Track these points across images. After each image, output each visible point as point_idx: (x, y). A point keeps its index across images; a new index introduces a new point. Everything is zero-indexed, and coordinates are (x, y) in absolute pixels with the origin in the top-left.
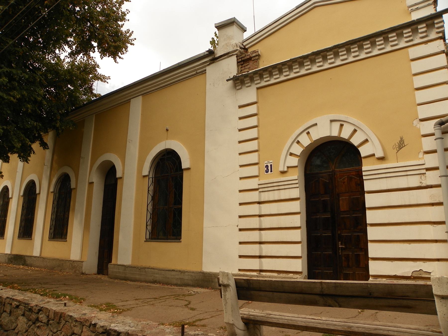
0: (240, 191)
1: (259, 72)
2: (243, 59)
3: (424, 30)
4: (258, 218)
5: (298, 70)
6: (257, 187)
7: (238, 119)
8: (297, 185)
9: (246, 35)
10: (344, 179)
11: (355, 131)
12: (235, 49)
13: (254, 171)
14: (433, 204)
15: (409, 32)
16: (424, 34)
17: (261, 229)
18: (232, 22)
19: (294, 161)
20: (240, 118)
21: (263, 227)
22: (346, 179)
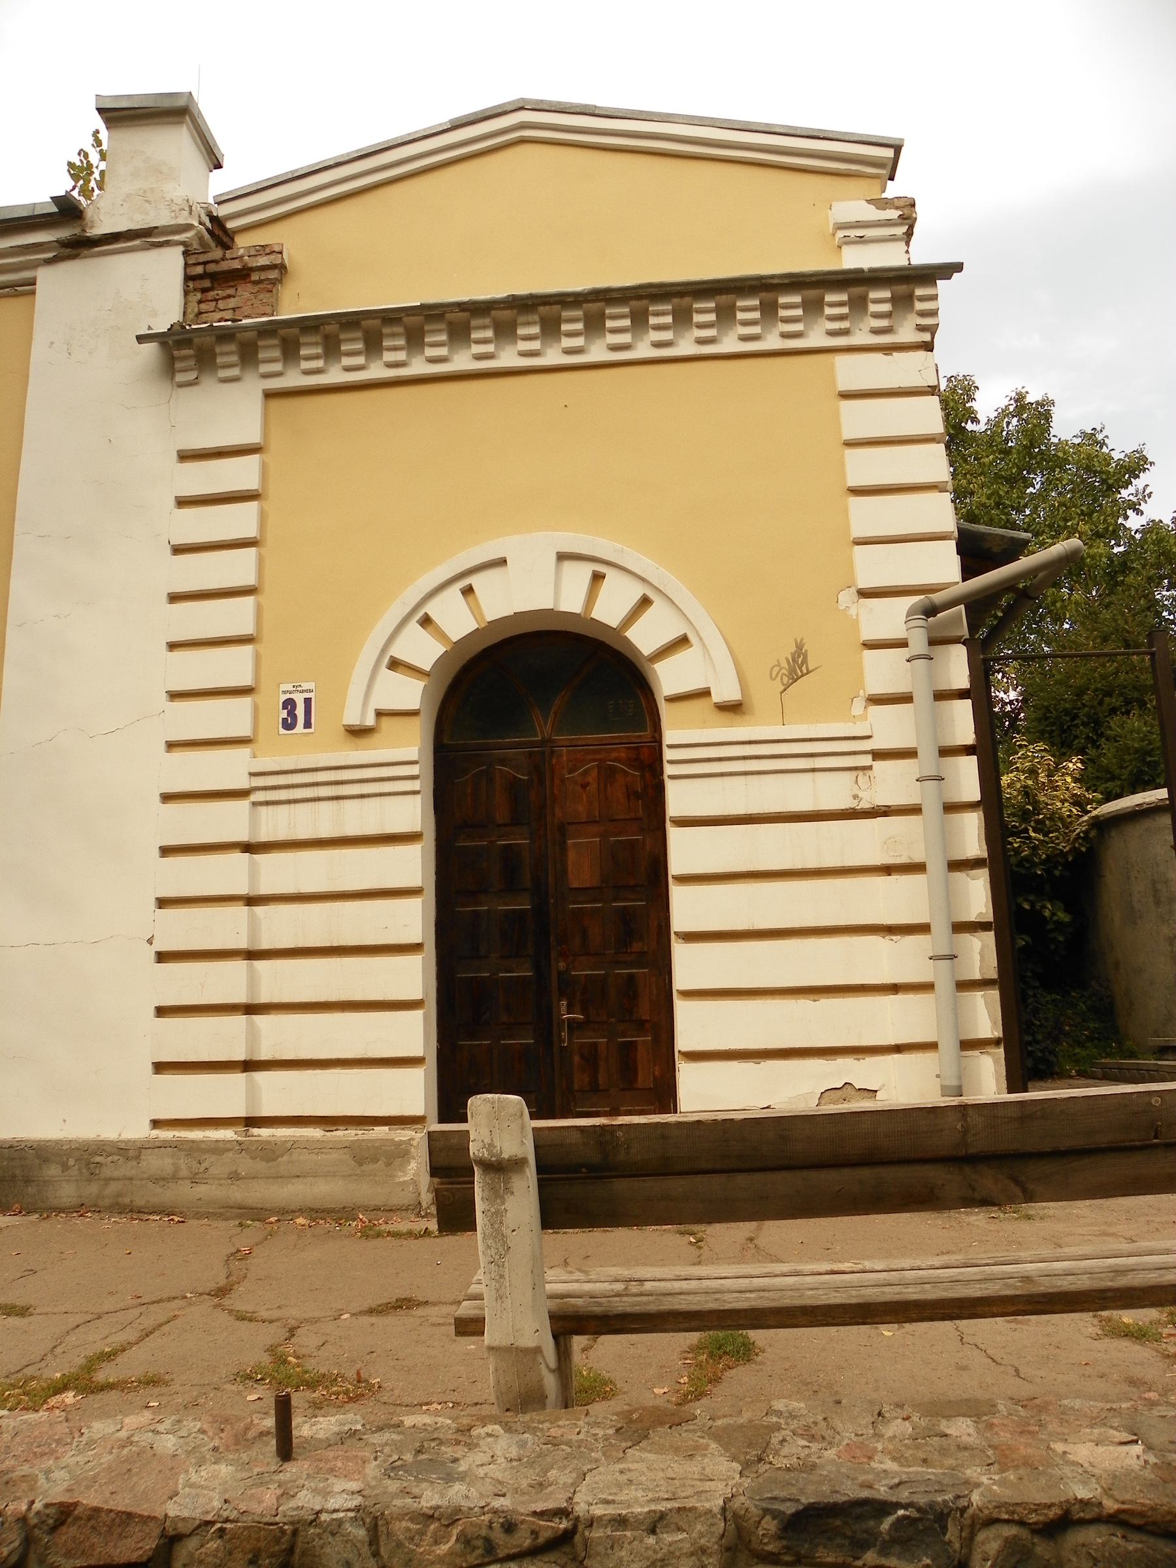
0: (167, 798)
1: (282, 332)
2: (212, 268)
3: (886, 307)
4: (242, 910)
5: (443, 351)
6: (243, 783)
7: (172, 502)
8: (416, 785)
9: (220, 183)
10: (586, 773)
11: (645, 602)
12: (181, 221)
13: (233, 717)
14: (888, 870)
15: (841, 304)
16: (884, 323)
17: (252, 955)
18: (173, 112)
19: (409, 693)
20: (183, 502)
21: (265, 945)
22: (594, 773)
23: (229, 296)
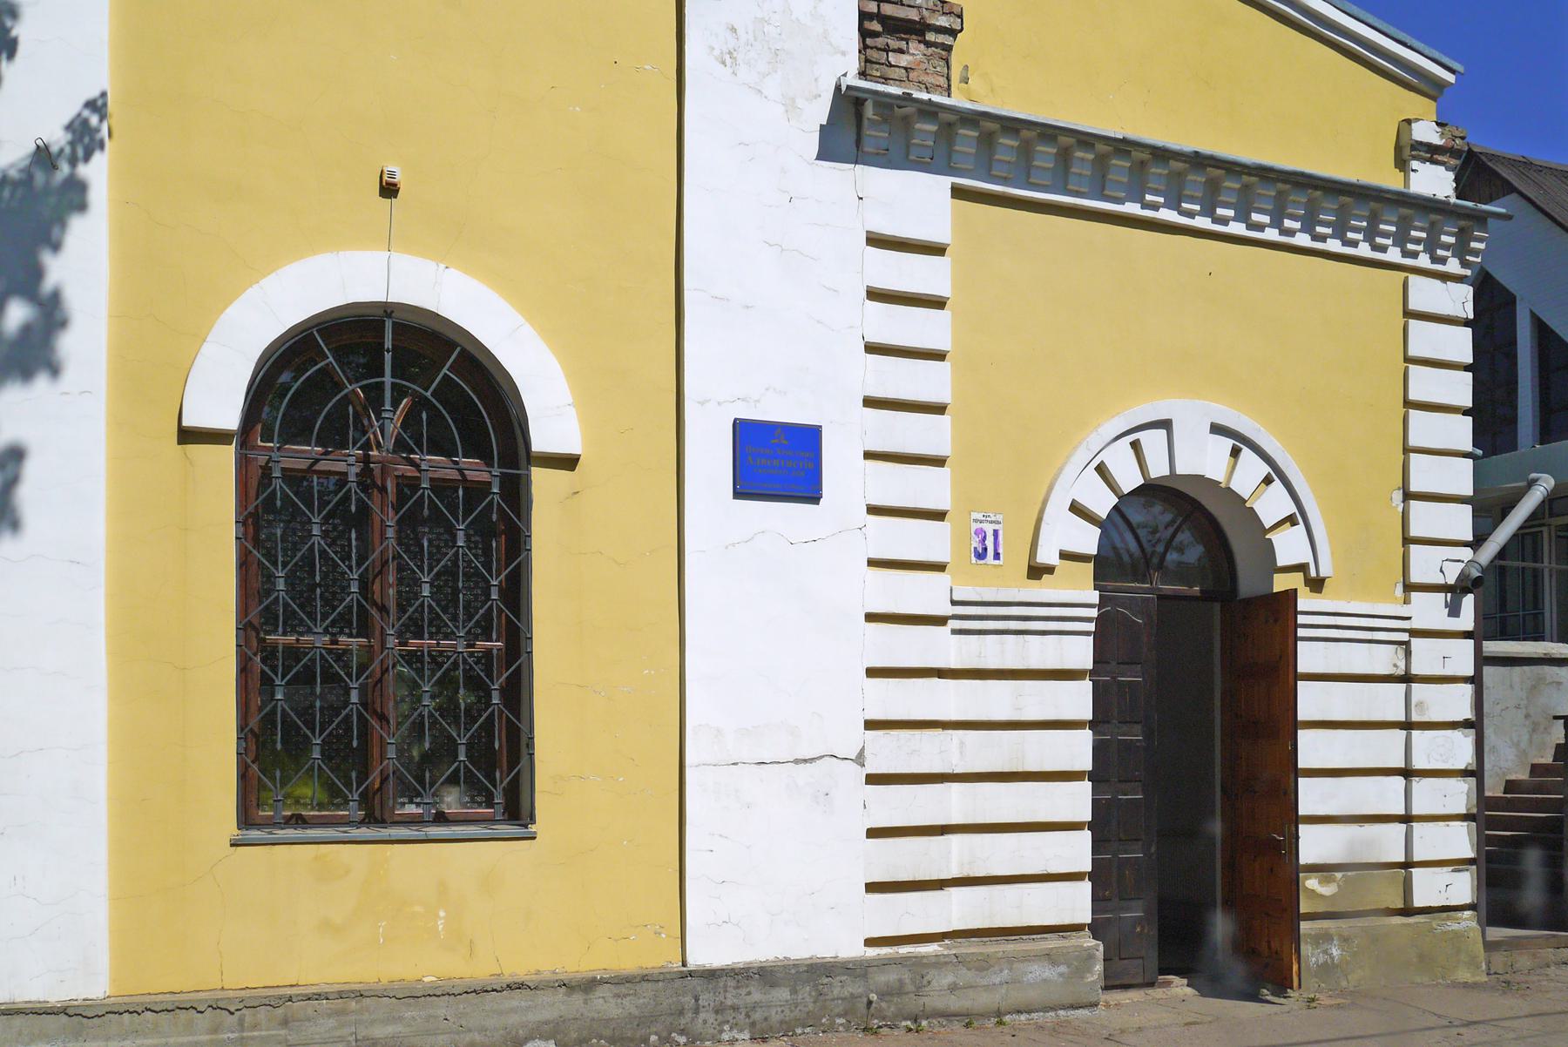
6: (946, 609)
20: (875, 295)
23: (901, 51)
